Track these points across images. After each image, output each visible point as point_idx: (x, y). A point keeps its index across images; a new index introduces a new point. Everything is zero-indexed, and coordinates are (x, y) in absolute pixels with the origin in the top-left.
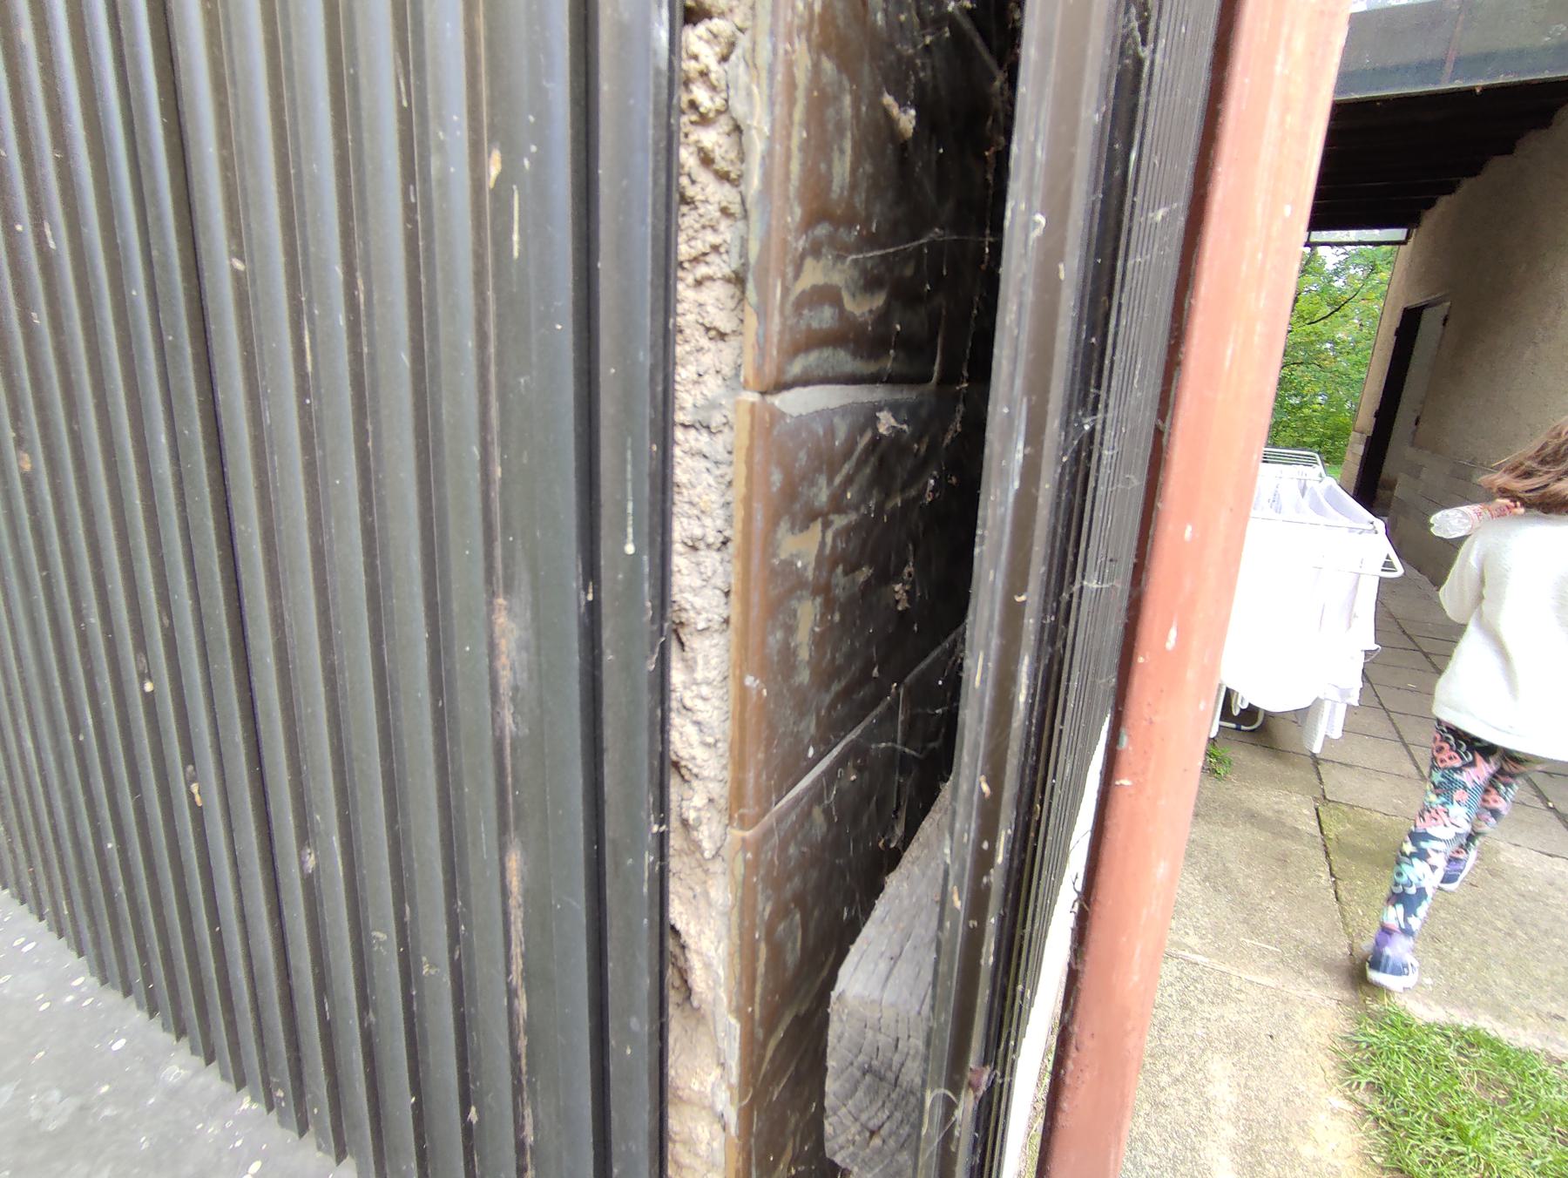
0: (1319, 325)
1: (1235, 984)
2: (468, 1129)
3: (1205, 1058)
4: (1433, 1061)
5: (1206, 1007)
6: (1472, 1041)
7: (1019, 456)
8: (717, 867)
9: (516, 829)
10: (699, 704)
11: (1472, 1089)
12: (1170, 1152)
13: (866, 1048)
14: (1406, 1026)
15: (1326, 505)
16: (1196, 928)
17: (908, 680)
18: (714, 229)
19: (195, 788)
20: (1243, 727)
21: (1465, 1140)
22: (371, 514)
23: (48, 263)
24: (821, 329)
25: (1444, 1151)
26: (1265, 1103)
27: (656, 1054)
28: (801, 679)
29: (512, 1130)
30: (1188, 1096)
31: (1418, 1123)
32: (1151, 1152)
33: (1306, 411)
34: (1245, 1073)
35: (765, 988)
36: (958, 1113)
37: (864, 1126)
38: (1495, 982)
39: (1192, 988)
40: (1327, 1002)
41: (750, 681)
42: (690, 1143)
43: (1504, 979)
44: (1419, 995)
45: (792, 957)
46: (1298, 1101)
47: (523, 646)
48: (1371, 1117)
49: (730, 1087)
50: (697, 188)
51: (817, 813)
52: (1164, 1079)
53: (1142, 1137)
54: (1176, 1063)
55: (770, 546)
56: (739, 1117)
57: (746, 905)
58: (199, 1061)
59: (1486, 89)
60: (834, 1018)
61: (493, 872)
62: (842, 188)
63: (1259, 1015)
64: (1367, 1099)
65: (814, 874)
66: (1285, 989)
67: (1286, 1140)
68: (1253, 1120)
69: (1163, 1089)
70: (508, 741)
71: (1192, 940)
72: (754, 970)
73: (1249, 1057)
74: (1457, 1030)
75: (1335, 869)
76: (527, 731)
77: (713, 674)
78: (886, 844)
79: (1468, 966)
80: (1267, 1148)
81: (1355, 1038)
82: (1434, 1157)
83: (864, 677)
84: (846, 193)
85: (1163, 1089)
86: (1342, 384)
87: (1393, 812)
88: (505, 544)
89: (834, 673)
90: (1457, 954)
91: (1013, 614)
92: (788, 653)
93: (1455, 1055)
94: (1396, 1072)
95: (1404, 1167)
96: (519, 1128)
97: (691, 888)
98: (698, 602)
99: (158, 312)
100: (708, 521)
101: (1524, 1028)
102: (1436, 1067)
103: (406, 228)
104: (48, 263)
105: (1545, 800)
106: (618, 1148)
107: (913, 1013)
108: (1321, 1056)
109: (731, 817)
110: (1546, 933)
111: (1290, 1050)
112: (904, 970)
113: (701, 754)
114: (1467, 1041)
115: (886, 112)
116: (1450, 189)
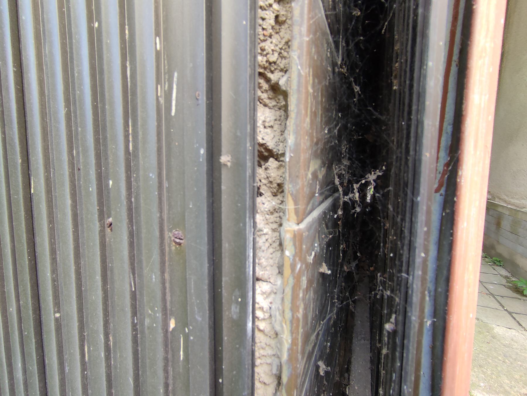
38: (503, 382)
43: (506, 381)
99: (12, 223)
103: (132, 334)
105: (503, 307)
110: (515, 360)
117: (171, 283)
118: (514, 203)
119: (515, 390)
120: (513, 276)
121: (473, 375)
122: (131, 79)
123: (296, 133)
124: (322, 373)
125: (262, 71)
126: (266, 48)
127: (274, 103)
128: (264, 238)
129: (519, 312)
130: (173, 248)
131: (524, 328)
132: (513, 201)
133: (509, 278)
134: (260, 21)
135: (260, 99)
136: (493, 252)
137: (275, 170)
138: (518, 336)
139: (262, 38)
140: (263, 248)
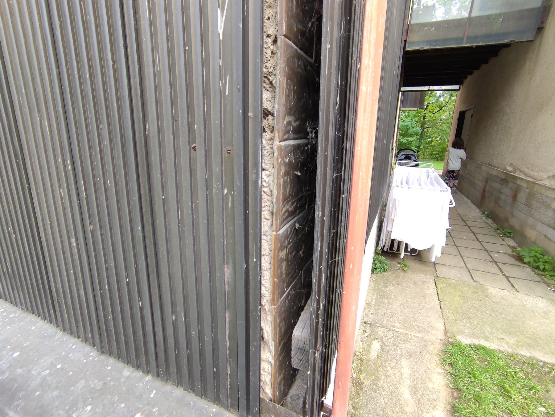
0: (436, 114)
1: (410, 337)
3: (401, 360)
4: (467, 355)
5: (401, 345)
6: (478, 348)
7: (320, 245)
10: (265, 283)
11: (478, 362)
12: (390, 390)
14: (460, 345)
15: (435, 182)
16: (398, 320)
17: (304, 269)
18: (266, 203)
20: (412, 254)
21: (475, 378)
25: (469, 381)
26: (418, 372)
30: (396, 372)
31: (462, 374)
32: (385, 390)
33: (433, 143)
35: (279, 336)
36: (316, 355)
37: (299, 359)
39: (397, 339)
40: (437, 340)
41: (275, 280)
42: (264, 369)
43: (488, 329)
44: (464, 336)
45: (283, 330)
46: (428, 371)
48: (449, 374)
49: (272, 356)
51: (287, 301)
52: (389, 368)
54: (392, 363)
56: (274, 362)
57: (275, 320)
59: (476, 47)
60: (293, 340)
63: (417, 346)
64: (448, 368)
65: (286, 313)
67: (425, 383)
69: (388, 371)
70: (226, 292)
71: (397, 324)
73: (414, 359)
74: (475, 345)
75: (440, 299)
76: (231, 290)
78: (301, 305)
79: (478, 326)
80: (419, 386)
81: (445, 351)
82: (466, 384)
83: (295, 271)
85: (388, 371)
86: (444, 134)
87: (457, 279)
88: (227, 256)
89: (289, 274)
90: (475, 323)
91: (320, 270)
92: (281, 273)
93: (474, 353)
94: (457, 359)
95: (458, 387)
101: (493, 343)
102: (468, 357)
105: (502, 272)
107: (307, 337)
108: (435, 357)
109: (272, 304)
110: (500, 314)
111: (426, 356)
112: (305, 330)
113: (265, 292)
114: (477, 348)
115: (296, 174)
116: (471, 74)
117: (225, 172)
118: (534, 175)
119: (494, 335)
120: (519, 246)
121: (461, 325)
122: (205, 77)
123: (279, 104)
124: (297, 228)
125: (266, 75)
126: (268, 65)
127: (272, 89)
128: (266, 151)
129: (515, 276)
130: (227, 155)
131: (516, 289)
132: (532, 173)
133: (515, 248)
134: (265, 54)
135: (265, 88)
136: (506, 225)
137: (272, 121)
138: (508, 295)
139: (266, 61)
140: (266, 155)
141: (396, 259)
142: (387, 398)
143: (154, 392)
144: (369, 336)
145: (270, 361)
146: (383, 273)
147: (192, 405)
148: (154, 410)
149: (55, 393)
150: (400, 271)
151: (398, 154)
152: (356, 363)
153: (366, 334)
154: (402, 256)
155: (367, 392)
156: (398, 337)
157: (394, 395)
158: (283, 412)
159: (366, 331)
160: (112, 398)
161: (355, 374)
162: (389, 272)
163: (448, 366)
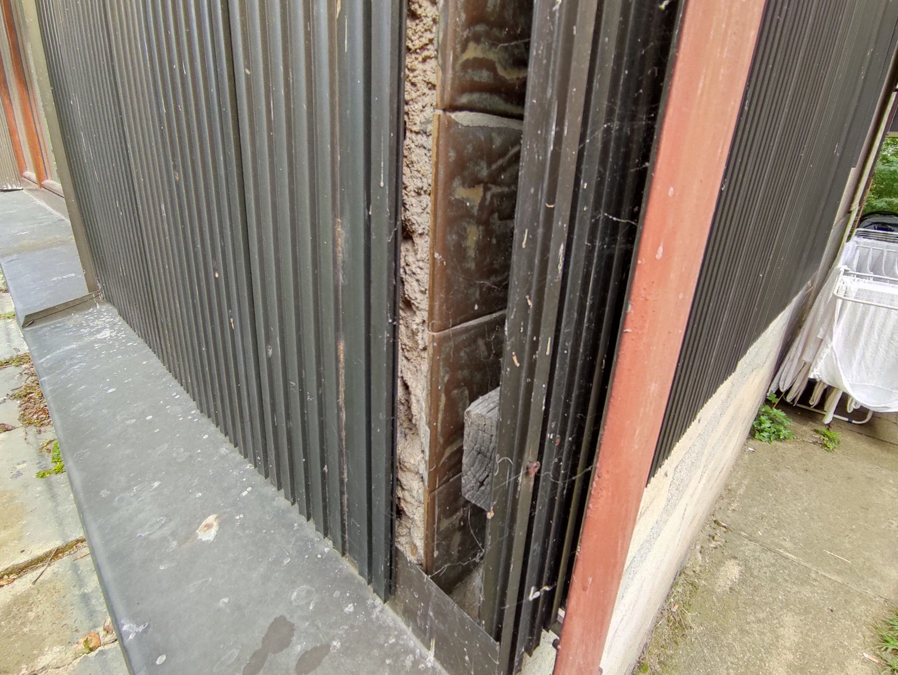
1: (813, 575)
2: (323, 473)
7: (553, 133)
8: (425, 355)
9: (343, 330)
13: (479, 440)
19: (232, 320)
22: (293, 184)
23: (183, 77)
24: (480, 82)
27: (390, 432)
28: (469, 266)
29: (337, 473)
30: (766, 631)
32: (733, 655)
34: (807, 627)
41: (436, 255)
46: (841, 650)
47: (347, 241)
48: (890, 669)
50: (422, 9)
53: (730, 647)
55: (448, 189)
57: (433, 371)
58: (232, 446)
61: (333, 350)
62: (495, 6)
64: (890, 658)
66: (849, 585)
68: (806, 654)
72: (438, 406)
73: (813, 618)
77: (424, 256)
81: (891, 623)
84: (497, 9)
88: (341, 191)
96: (341, 473)
97: (416, 367)
98: (419, 220)
100: (424, 180)
104: (183, 77)
106: (374, 476)
141: (810, 423)
142: (734, 669)
143: (249, 489)
144: (719, 548)
145: (421, 472)
146: (774, 443)
147: (295, 528)
148: (238, 517)
149: (128, 452)
150: (816, 447)
151: (862, 220)
152: (682, 587)
153: (714, 543)
154: (828, 419)
155: (695, 645)
156: (785, 568)
157: (752, 669)
158: (434, 594)
159: (715, 538)
160: (190, 480)
161: (676, 606)
162: (790, 443)
163: (890, 653)
